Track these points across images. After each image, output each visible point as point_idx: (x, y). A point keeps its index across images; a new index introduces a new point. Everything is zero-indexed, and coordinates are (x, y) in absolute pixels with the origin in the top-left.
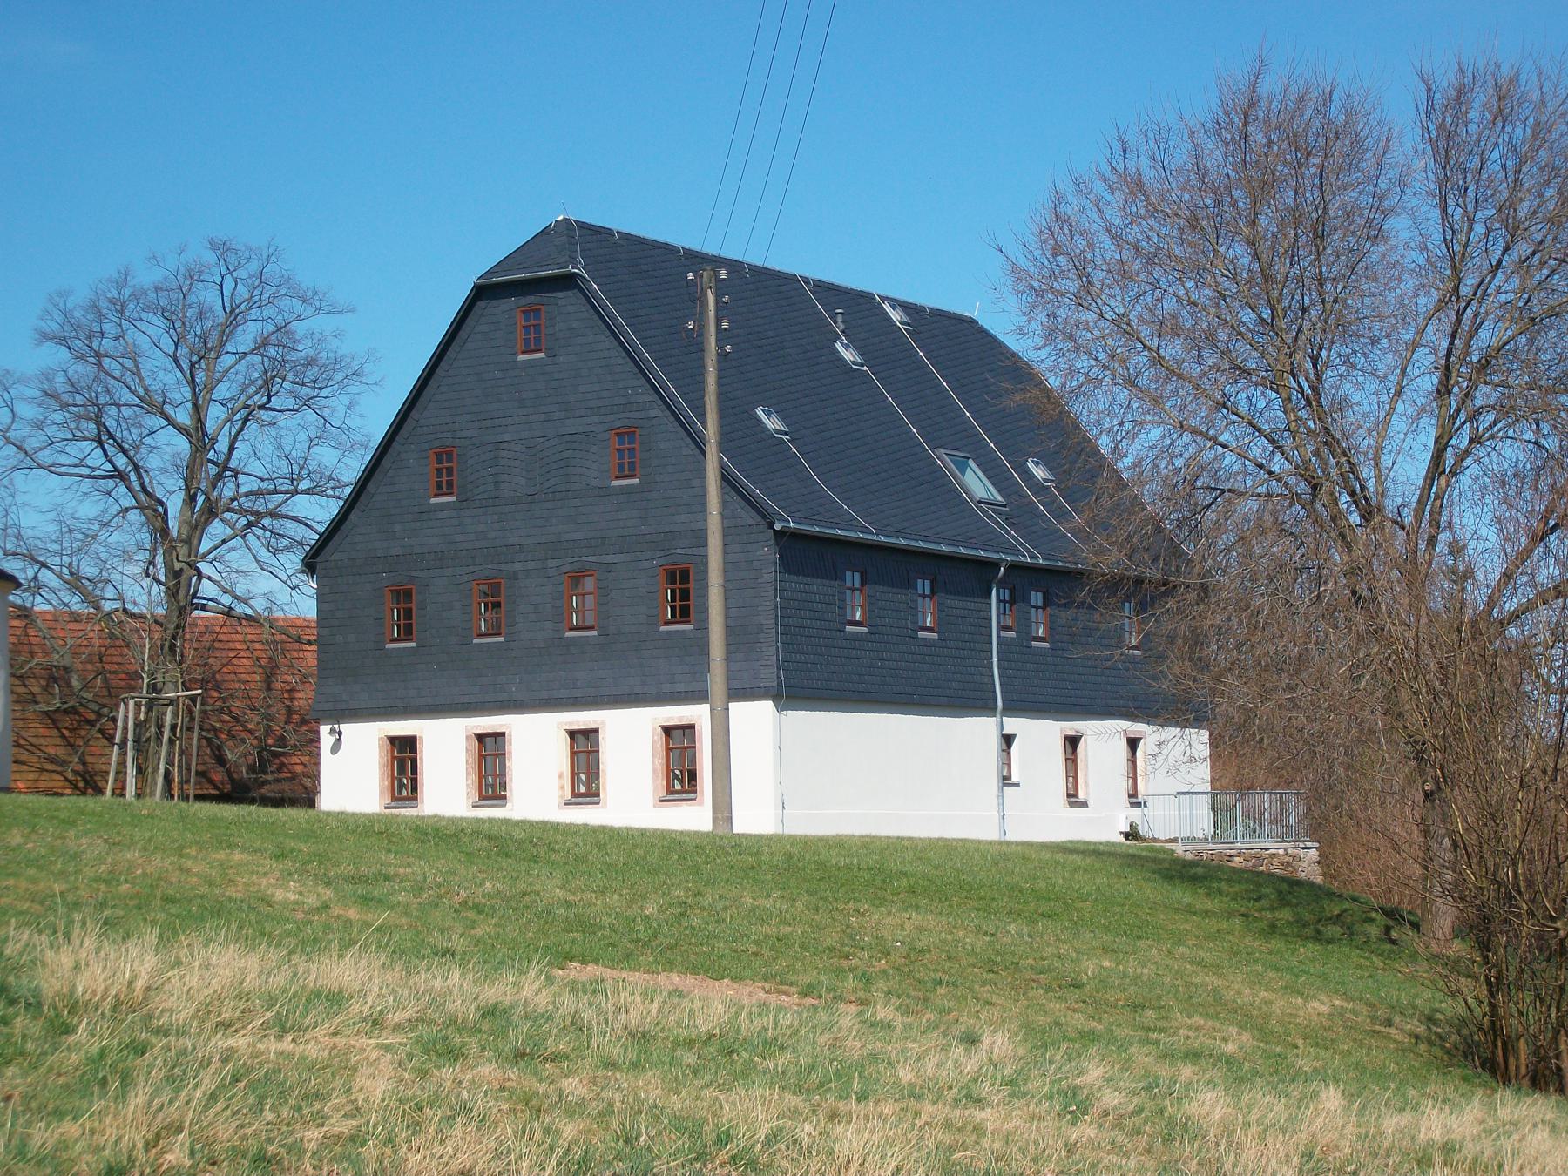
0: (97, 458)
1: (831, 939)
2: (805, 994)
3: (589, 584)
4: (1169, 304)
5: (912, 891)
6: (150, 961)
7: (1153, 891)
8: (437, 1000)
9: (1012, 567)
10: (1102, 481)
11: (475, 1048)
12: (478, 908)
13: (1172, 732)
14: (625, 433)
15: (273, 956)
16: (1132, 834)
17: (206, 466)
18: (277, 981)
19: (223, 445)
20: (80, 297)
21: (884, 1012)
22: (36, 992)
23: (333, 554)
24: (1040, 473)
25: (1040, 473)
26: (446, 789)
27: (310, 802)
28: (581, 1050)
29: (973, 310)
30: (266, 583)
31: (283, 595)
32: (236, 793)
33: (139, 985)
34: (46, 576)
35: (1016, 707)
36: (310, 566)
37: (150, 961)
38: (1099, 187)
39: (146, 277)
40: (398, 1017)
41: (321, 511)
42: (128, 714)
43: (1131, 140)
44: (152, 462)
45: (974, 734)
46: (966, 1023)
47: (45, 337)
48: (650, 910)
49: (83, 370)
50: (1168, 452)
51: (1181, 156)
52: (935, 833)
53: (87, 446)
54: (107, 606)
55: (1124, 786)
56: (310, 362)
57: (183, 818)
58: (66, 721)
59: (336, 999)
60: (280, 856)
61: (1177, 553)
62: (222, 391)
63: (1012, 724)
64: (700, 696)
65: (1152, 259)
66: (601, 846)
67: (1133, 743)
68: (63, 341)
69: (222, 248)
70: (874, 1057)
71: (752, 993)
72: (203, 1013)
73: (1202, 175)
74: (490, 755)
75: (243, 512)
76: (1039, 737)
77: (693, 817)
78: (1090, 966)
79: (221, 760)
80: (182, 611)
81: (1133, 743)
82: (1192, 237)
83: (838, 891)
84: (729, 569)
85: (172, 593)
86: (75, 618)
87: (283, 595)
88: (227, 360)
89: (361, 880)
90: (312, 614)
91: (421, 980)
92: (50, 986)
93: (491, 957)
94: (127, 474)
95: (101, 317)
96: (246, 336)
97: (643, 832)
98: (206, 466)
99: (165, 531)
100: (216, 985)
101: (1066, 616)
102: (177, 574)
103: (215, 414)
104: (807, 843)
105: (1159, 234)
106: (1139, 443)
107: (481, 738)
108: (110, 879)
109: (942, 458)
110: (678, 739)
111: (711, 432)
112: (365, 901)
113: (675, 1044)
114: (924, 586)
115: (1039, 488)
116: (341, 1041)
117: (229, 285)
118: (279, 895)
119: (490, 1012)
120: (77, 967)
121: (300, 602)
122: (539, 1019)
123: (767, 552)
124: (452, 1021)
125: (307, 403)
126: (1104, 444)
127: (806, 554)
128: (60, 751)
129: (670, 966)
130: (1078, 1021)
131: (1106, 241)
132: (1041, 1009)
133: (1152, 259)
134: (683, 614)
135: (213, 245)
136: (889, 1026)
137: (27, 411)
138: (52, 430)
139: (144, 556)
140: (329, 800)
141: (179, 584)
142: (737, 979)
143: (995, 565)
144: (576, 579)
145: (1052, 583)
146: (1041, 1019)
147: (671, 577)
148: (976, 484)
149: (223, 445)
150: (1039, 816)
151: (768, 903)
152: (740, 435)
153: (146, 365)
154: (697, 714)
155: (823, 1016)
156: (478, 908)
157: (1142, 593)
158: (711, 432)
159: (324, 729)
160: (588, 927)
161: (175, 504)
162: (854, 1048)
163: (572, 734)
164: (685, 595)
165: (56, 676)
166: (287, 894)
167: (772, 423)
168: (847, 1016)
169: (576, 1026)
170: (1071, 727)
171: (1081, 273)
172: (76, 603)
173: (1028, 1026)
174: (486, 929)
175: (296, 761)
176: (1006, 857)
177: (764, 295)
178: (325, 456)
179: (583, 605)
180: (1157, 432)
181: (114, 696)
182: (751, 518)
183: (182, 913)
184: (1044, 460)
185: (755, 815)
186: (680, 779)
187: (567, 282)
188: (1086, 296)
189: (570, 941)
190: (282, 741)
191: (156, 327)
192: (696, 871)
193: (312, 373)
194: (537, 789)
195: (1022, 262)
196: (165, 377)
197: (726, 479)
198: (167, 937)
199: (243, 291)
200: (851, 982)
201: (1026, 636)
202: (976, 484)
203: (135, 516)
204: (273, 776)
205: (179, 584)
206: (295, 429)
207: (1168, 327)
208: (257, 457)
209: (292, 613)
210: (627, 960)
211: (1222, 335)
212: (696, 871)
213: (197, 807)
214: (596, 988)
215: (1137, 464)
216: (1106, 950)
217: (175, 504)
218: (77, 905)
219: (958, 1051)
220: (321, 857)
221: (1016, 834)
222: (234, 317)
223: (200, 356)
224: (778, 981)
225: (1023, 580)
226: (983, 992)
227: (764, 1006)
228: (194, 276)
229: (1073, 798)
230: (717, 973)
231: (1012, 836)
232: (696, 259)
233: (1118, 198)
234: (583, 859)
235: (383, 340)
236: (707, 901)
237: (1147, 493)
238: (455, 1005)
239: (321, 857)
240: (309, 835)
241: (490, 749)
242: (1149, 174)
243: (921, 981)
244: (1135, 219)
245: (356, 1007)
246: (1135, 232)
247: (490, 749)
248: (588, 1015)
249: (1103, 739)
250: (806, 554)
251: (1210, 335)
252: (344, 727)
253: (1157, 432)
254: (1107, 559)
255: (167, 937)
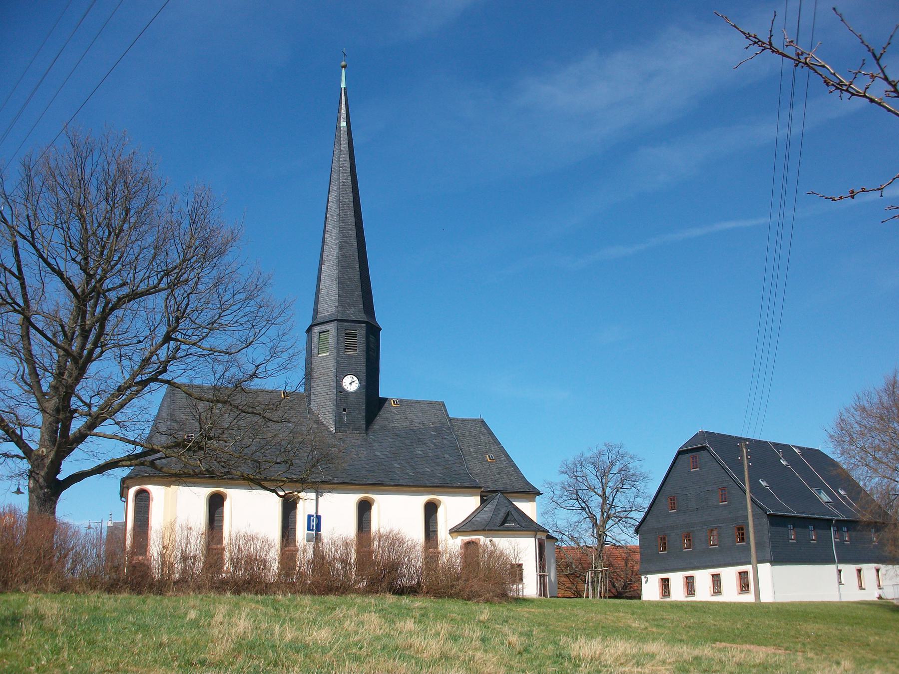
0: (577, 504)
1: (792, 633)
2: (786, 649)
3: (715, 533)
4: (877, 442)
5: (815, 617)
6: (600, 646)
7: (888, 615)
8: (680, 655)
9: (837, 521)
10: (862, 494)
11: (692, 669)
12: (690, 627)
13: (890, 567)
14: (723, 489)
15: (633, 644)
16: (880, 598)
17: (607, 505)
18: (635, 651)
19: (611, 499)
20: (570, 460)
21: (810, 655)
22: (569, 656)
23: (643, 528)
24: (842, 493)
25: (842, 493)
26: (678, 593)
27: (639, 597)
28: (723, 669)
29: (820, 448)
30: (625, 536)
31: (629, 539)
32: (618, 596)
33: (598, 653)
34: (564, 537)
35: (842, 561)
36: (637, 532)
37: (600, 646)
38: (853, 410)
39: (588, 454)
40: (670, 660)
41: (639, 516)
42: (589, 575)
43: (861, 396)
44: (592, 505)
45: (830, 570)
46: (836, 657)
47: (562, 472)
48: (739, 626)
49: (572, 481)
50: (881, 484)
51: (875, 400)
52: (820, 600)
53: (574, 501)
54: (582, 545)
55: (875, 583)
56: (633, 475)
57: (605, 603)
58: (571, 577)
59: (652, 656)
60: (633, 614)
61: (886, 514)
62: (610, 484)
63: (841, 566)
64: (749, 563)
65: (870, 430)
66: (723, 607)
67: (878, 570)
68: (566, 473)
69: (608, 445)
70: (809, 669)
71: (771, 650)
72: (617, 659)
73: (882, 404)
74: (690, 582)
75: (617, 517)
76: (849, 570)
77: (749, 598)
78: (872, 639)
79: (614, 586)
80: (602, 546)
81: (878, 570)
82: (881, 422)
83: (793, 617)
84: (755, 526)
85: (599, 541)
86: (573, 548)
87: (629, 539)
88: (611, 476)
89: (657, 620)
90: (638, 544)
91: (675, 649)
92: (573, 653)
93: (695, 641)
94: (585, 508)
95: (576, 466)
96: (616, 469)
97: (735, 603)
98: (607, 505)
99: (596, 523)
100: (619, 652)
101: (854, 534)
102: (600, 535)
103: (608, 490)
104: (782, 604)
105: (871, 422)
106: (870, 481)
107: (687, 578)
108: (587, 622)
109: (814, 491)
110: (743, 576)
111: (747, 488)
112: (658, 626)
113: (750, 667)
114: (812, 528)
115: (843, 497)
116: (654, 668)
117: (610, 455)
118: (633, 625)
119: (696, 658)
120: (580, 648)
121: (635, 541)
122: (710, 660)
123: (765, 520)
124: (685, 661)
125: (633, 486)
126: (861, 484)
127: (777, 520)
128: (570, 585)
129: (746, 642)
130: (870, 656)
131: (856, 426)
132: (858, 653)
133: (870, 430)
134: (742, 540)
135: (605, 445)
136: (812, 659)
137: (558, 493)
138: (564, 497)
139: (591, 531)
140: (645, 597)
141: (601, 537)
142: (766, 646)
143: (832, 520)
144: (711, 531)
145: (850, 524)
146: (858, 656)
147: (738, 530)
148: (824, 497)
149: (611, 499)
150: (851, 593)
151: (773, 623)
152: (756, 488)
153: (589, 478)
154: (748, 568)
155: (792, 657)
156: (690, 627)
157: (878, 527)
158: (747, 488)
159: (643, 577)
160: (721, 631)
161: (599, 516)
162: (803, 666)
163: (713, 575)
164: (743, 534)
165: (568, 565)
166: (635, 625)
167: (764, 484)
168: (799, 657)
169: (721, 662)
170: (858, 566)
171: (850, 435)
172: (573, 544)
173: (855, 659)
174: (692, 633)
175: (635, 586)
176: (842, 606)
177: (758, 446)
178: (639, 500)
179: (713, 539)
180: (877, 479)
181: (585, 569)
182: (760, 511)
183: (608, 631)
184: (844, 489)
185: (767, 597)
186: (744, 586)
187: (704, 448)
188: (852, 441)
189: (717, 636)
190: (631, 580)
191: (591, 468)
192: (751, 614)
193: (634, 478)
194: (704, 592)
195: (832, 433)
196: (595, 482)
197: (752, 501)
198: (604, 638)
199: (614, 456)
200: (799, 646)
201: (843, 540)
202: (824, 497)
203: (588, 520)
204: (627, 591)
205: (601, 537)
206: (630, 493)
207: (877, 448)
208: (621, 502)
209: (632, 544)
210: (733, 641)
211: (893, 450)
212: (751, 614)
213: (612, 601)
214: (725, 649)
215: (871, 489)
216: (876, 634)
217: (599, 516)
218: (578, 629)
219: (834, 667)
220: (644, 614)
221: (844, 599)
222: (612, 464)
223: (603, 475)
224: (778, 646)
225: (840, 524)
226: (840, 648)
227: (774, 654)
228: (601, 453)
229: (861, 587)
230: (760, 644)
231: (843, 600)
232: (739, 439)
233: (859, 413)
234: (718, 612)
235: (654, 468)
236: (755, 623)
237: (875, 497)
238: (686, 656)
239: (644, 614)
240: (641, 608)
241: (690, 581)
242: (867, 405)
243: (820, 645)
244: (864, 418)
245: (657, 657)
246: (864, 422)
247: (690, 581)
248: (724, 658)
249: (868, 569)
250: (777, 520)
251: (890, 450)
252: (648, 576)
253: (877, 479)
254: (866, 517)
255: (604, 638)
